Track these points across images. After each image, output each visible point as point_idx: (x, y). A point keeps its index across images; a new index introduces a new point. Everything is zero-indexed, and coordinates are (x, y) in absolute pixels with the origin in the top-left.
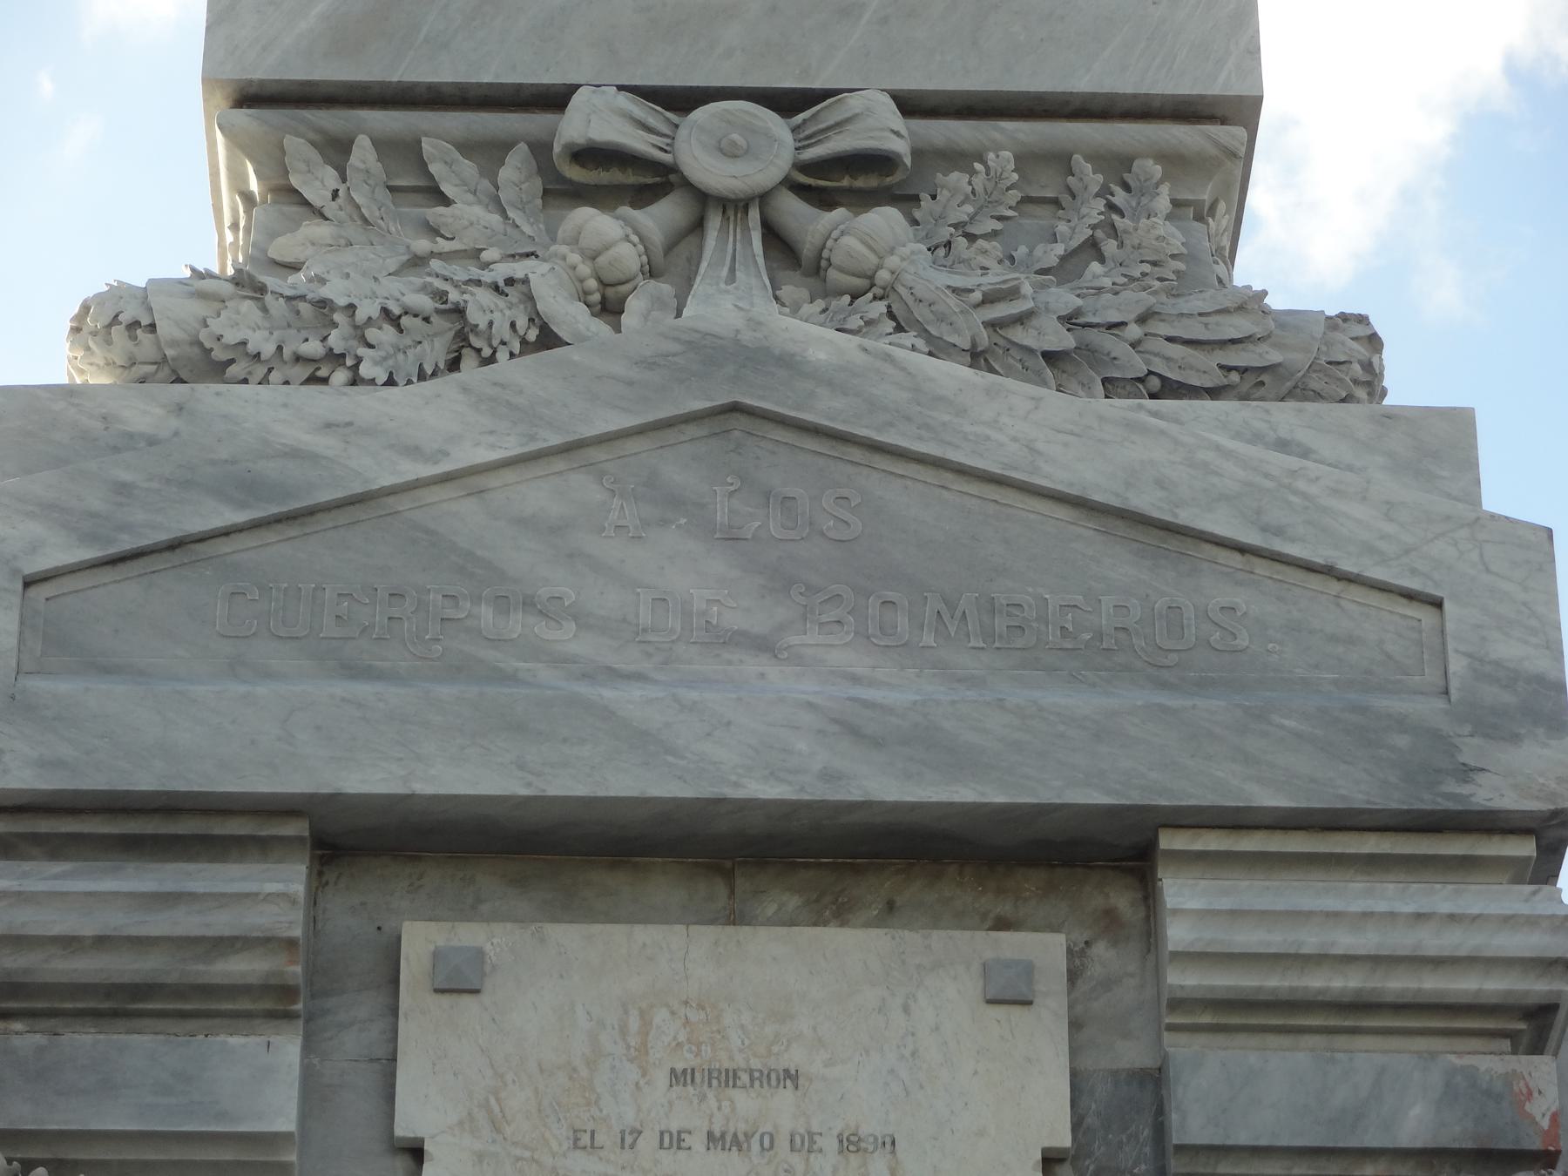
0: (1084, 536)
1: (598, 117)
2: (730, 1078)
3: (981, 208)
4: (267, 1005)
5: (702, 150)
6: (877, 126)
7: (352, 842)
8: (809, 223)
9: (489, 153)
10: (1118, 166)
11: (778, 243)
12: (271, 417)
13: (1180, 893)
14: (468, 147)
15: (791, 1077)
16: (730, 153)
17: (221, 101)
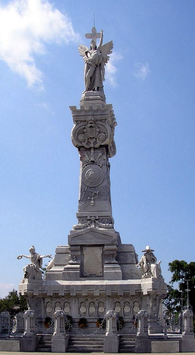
2: (92, 252)
6: (97, 218)
7: (82, 246)
11: (95, 222)
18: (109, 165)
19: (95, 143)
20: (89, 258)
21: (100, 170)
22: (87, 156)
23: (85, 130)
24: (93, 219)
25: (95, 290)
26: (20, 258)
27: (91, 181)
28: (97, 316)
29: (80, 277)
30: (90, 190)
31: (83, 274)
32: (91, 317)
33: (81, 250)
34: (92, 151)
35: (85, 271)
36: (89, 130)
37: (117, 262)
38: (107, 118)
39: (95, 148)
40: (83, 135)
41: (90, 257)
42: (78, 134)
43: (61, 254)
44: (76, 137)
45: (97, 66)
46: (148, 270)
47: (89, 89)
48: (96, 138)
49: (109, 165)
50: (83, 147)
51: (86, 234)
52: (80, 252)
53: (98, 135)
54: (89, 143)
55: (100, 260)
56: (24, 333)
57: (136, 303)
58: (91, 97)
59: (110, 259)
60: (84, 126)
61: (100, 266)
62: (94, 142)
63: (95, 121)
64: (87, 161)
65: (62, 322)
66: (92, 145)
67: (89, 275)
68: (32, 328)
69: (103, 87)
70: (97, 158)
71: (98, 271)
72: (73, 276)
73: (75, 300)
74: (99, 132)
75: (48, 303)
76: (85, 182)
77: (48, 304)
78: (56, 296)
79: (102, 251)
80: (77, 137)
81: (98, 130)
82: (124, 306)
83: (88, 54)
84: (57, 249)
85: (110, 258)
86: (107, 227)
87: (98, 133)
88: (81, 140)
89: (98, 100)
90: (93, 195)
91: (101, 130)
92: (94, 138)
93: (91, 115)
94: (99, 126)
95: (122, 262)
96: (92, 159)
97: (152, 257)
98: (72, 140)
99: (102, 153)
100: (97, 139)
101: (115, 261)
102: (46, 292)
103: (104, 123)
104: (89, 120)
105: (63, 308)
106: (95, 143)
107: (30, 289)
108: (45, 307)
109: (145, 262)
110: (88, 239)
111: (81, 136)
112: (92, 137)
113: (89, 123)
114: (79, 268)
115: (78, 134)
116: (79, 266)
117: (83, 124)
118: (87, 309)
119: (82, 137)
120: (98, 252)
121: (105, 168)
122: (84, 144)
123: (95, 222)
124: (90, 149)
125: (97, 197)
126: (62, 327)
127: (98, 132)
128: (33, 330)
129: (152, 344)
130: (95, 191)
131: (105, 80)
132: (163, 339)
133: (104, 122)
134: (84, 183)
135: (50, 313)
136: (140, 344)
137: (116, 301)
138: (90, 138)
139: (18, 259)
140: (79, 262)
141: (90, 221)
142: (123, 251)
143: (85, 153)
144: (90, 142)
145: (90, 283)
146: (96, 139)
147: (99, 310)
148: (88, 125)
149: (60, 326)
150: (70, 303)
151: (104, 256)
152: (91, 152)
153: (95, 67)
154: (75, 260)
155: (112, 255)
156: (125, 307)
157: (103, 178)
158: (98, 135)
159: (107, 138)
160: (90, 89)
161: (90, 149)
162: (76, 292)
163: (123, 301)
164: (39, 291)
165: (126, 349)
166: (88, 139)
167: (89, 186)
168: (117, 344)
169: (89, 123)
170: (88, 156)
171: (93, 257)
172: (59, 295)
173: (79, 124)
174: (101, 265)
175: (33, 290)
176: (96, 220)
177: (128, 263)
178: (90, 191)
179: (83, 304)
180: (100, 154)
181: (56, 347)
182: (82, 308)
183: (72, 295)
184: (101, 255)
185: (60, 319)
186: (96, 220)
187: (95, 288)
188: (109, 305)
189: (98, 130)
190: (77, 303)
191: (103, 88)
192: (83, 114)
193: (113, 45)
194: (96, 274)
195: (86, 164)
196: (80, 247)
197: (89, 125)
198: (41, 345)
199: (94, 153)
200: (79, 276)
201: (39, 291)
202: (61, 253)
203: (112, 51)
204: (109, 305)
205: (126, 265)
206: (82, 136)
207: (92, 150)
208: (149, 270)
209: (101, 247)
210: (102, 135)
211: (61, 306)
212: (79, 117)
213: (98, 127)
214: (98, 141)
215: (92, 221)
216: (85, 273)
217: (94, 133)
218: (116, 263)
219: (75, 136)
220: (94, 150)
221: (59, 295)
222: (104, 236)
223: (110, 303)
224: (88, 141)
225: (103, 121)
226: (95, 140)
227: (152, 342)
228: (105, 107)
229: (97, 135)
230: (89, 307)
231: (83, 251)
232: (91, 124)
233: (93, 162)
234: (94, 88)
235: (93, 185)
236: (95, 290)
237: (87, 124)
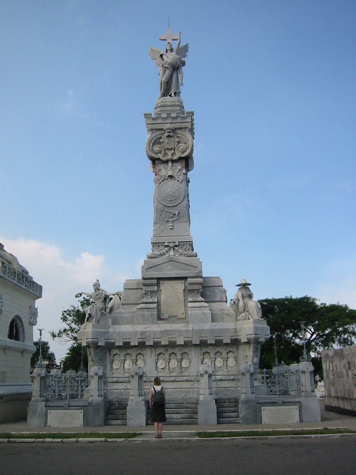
0: (185, 265)
1: (166, 244)
2: (172, 287)
3: (179, 93)
4: (12, 349)
5: (170, 245)
6: (177, 244)
7: (159, 279)
8: (175, 248)
9: (162, 245)
10: (187, 244)
11: (174, 249)
12: (155, 261)
13: (188, 279)
14: (161, 245)
15: (174, 287)
16: (172, 245)
17: (324, 408)
18: (188, 181)
19: (173, 154)
20: (168, 295)
21: (180, 187)
22: (163, 170)
23: (161, 140)
24: (172, 245)
25: (179, 336)
26: (79, 295)
27: (169, 200)
28: (180, 373)
29: (158, 320)
30: (167, 210)
31: (160, 317)
32: (172, 374)
33: (158, 284)
34: (170, 164)
35: (162, 312)
36: (166, 140)
37: (203, 299)
38: (188, 126)
39: (173, 161)
40: (159, 146)
41: (170, 294)
42: (154, 144)
43: (131, 290)
44: (151, 148)
45: (174, 69)
46: (245, 310)
47: (164, 95)
48: (174, 148)
49: (188, 181)
50: (159, 159)
51: (164, 264)
52: (156, 287)
53: (177, 145)
54: (165, 154)
55: (182, 298)
56: (31, 399)
57: (230, 354)
58: (168, 103)
59: (195, 295)
60: (160, 136)
61: (182, 304)
62: (172, 153)
63: (174, 130)
64: (164, 176)
65: (141, 383)
66: (169, 157)
67: (168, 318)
68: (100, 392)
69: (180, 92)
70: (175, 172)
71: (180, 312)
72: (148, 319)
73: (151, 353)
74: (179, 143)
75: (115, 355)
76: (161, 201)
77: (115, 357)
78: (127, 346)
79: (184, 285)
80: (152, 148)
81: (177, 139)
82: (215, 358)
83: (164, 57)
84: (125, 284)
85: (194, 294)
86: (190, 255)
87: (177, 143)
88: (157, 152)
89: (168, 106)
90: (171, 216)
91: (181, 140)
92: (171, 149)
93: (170, 123)
94: (178, 135)
95: (210, 300)
96: (170, 173)
97: (248, 293)
98: (147, 151)
99: (181, 166)
100: (176, 150)
101: (200, 299)
102: (114, 340)
103: (184, 132)
104: (167, 129)
105: (135, 362)
106: (173, 154)
107: (95, 338)
108: (112, 362)
109: (241, 299)
110: (167, 270)
111: (157, 147)
112: (170, 148)
113: (167, 132)
114: (156, 308)
115: (154, 144)
116: (155, 305)
117: (158, 134)
118: (167, 363)
119: (158, 148)
120: (179, 286)
121: (184, 183)
122: (160, 156)
123: (174, 249)
124: (167, 162)
125: (176, 218)
126: (100, 389)
127: (177, 142)
128: (102, 393)
129: (262, 411)
130: (173, 211)
131: (183, 85)
132: (276, 403)
133: (184, 131)
134: (161, 202)
135: (117, 369)
136: (246, 411)
137: (204, 352)
138: (168, 149)
139: (77, 297)
140: (156, 300)
141: (168, 248)
142: (208, 286)
143: (162, 166)
144: (167, 154)
145: (171, 327)
146: (174, 150)
147: (182, 365)
148: (166, 135)
149: (138, 388)
150: (144, 355)
151: (188, 291)
152: (169, 166)
153: (173, 70)
154: (150, 297)
155: (198, 290)
156: (217, 360)
157: (183, 196)
158: (177, 145)
159: (188, 149)
160: (165, 95)
161: (167, 162)
162: (154, 339)
163: (135, 353)
164: (105, 339)
165: (227, 419)
166: (165, 150)
167: (166, 205)
168: (145, 413)
169: (167, 132)
170: (165, 170)
171: (171, 294)
172: (132, 344)
173: (154, 134)
174: (184, 304)
175: (98, 339)
176: (176, 246)
177: (216, 300)
178: (168, 212)
179: (162, 356)
180: (179, 168)
181: (134, 418)
182: (160, 361)
183: (148, 344)
184: (183, 291)
185: (138, 378)
186: (176, 246)
187: (178, 335)
188: (195, 357)
189: (177, 139)
190: (153, 355)
191: (181, 93)
192: (159, 121)
193: (188, 48)
194: (177, 316)
195: (160, 181)
196: (156, 280)
197: (166, 134)
198: (111, 416)
199: (172, 166)
200: (156, 320)
201: (105, 339)
202: (130, 289)
203: (187, 55)
204: (195, 357)
205: (214, 303)
206: (158, 147)
207: (169, 163)
208: (247, 310)
209: (183, 281)
210: (181, 146)
211: (132, 359)
212: (155, 125)
213: (178, 137)
214: (176, 153)
215: (170, 247)
216: (163, 315)
217: (172, 143)
218: (203, 300)
219: (150, 147)
220: (172, 163)
221: (132, 344)
222: (187, 267)
223: (197, 354)
224: (165, 152)
225: (183, 130)
226: (173, 151)
227: (262, 408)
228: (186, 114)
229: (175, 146)
230: (170, 359)
231: (160, 286)
232: (169, 134)
233: (171, 177)
234: (170, 94)
235: (171, 204)
236: (179, 336)
237: (164, 133)
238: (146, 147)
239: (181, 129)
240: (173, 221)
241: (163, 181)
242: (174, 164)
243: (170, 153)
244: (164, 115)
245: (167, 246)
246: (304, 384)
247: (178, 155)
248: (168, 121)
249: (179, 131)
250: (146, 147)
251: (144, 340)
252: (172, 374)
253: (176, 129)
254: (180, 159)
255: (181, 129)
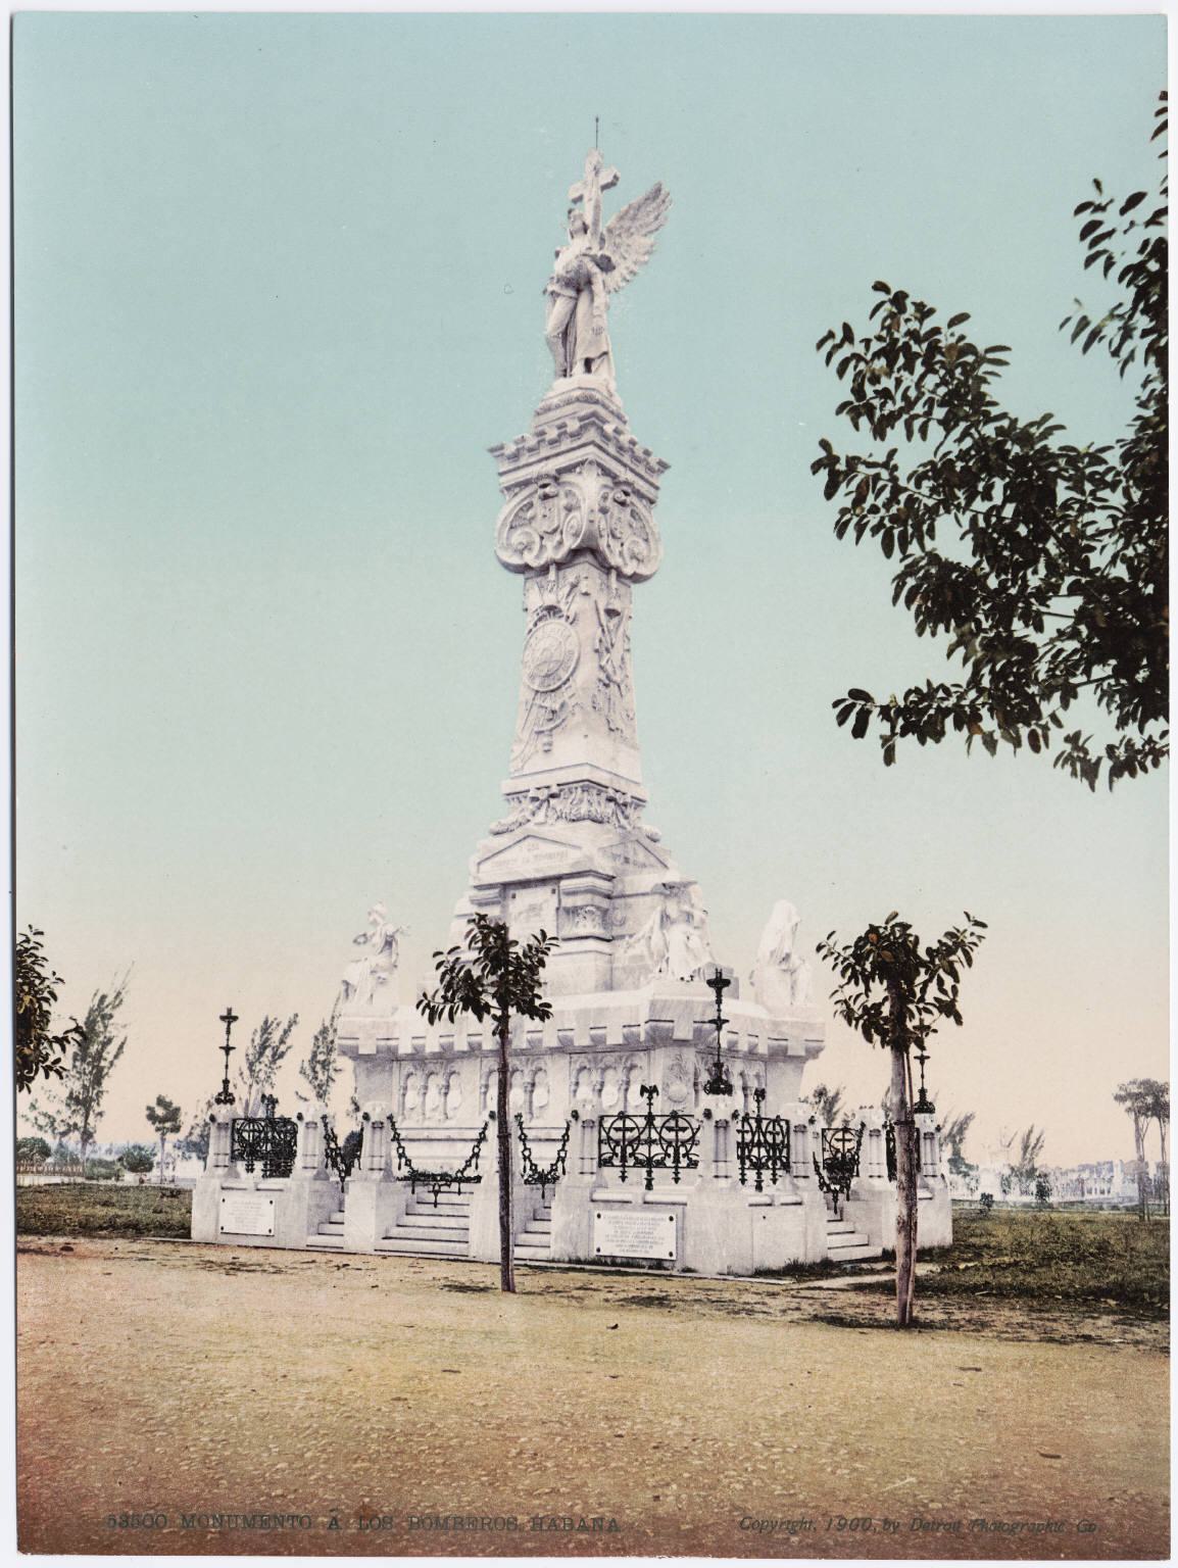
1: (530, 794)
6: (555, 790)
92: (555, 531)
146: (562, 533)
166: (542, 538)
176: (553, 796)
186: (553, 796)
192: (545, 452)
233: (552, 610)
238: (1068, 320)
239: (570, 469)
240: (551, 730)
241: (536, 625)
242: (561, 573)
243: (550, 543)
244: (553, 434)
245: (535, 799)
246: (441, 1198)
247: (571, 543)
248: (563, 447)
249: (566, 478)
250: (1068, 320)
251: (451, 1040)
252: (448, 1124)
253: (561, 471)
254: (575, 553)
255: (570, 469)
